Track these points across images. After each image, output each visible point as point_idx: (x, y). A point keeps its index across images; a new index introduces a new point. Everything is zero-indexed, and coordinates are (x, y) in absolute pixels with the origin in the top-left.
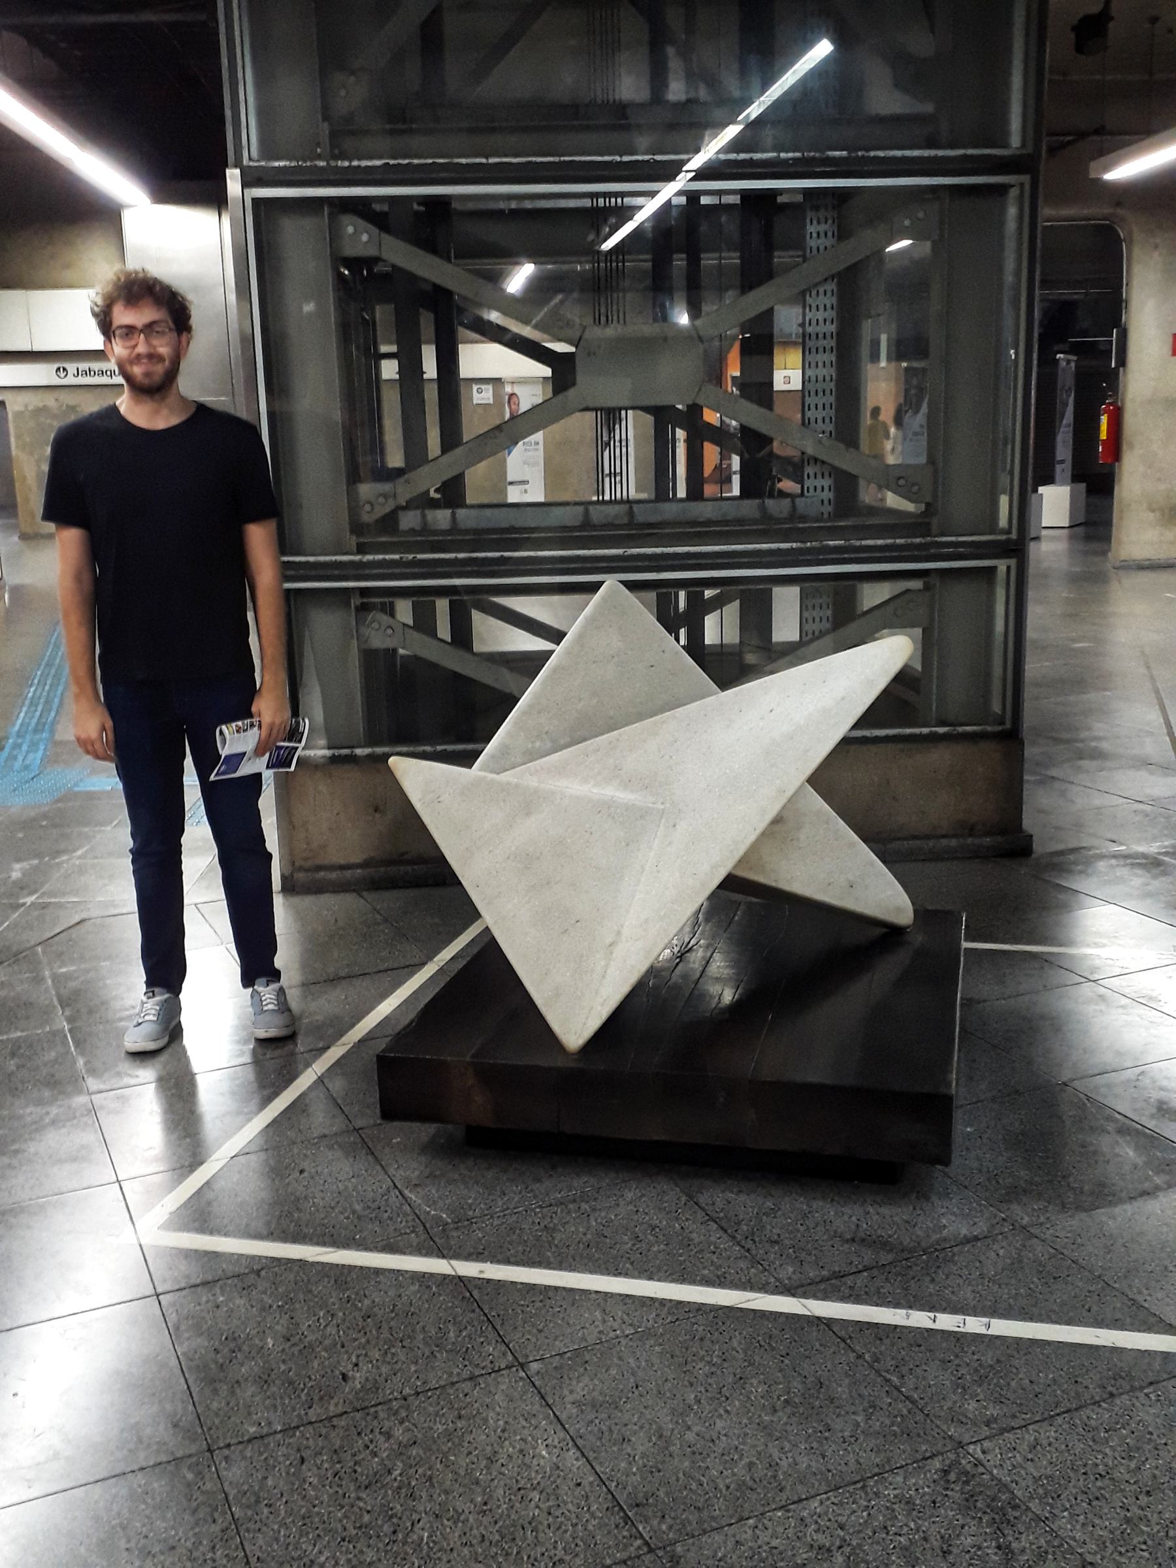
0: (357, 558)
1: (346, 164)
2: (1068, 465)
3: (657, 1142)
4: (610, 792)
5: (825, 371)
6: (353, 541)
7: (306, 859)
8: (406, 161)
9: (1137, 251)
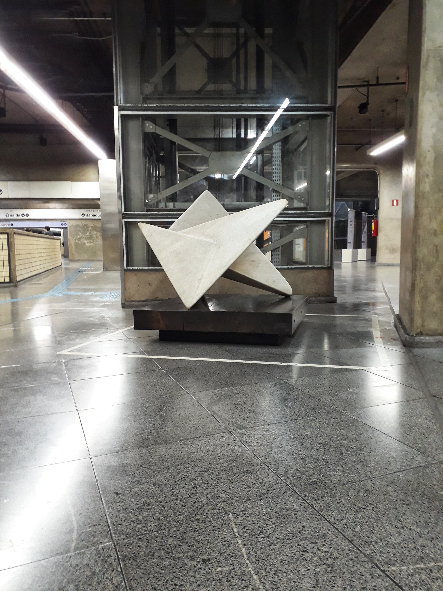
0: (146, 213)
1: (146, 105)
2: (366, 243)
3: (211, 332)
4: (202, 238)
5: (278, 167)
6: (145, 209)
7: (129, 299)
8: (163, 105)
9: (381, 176)
